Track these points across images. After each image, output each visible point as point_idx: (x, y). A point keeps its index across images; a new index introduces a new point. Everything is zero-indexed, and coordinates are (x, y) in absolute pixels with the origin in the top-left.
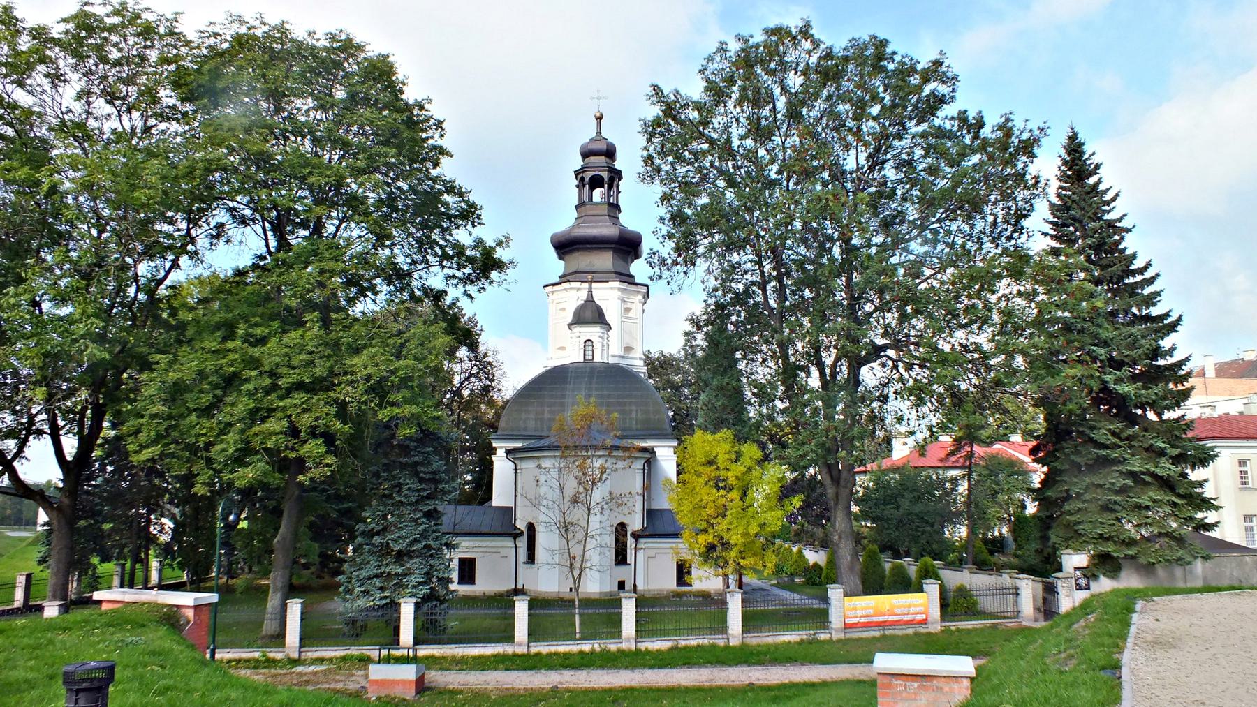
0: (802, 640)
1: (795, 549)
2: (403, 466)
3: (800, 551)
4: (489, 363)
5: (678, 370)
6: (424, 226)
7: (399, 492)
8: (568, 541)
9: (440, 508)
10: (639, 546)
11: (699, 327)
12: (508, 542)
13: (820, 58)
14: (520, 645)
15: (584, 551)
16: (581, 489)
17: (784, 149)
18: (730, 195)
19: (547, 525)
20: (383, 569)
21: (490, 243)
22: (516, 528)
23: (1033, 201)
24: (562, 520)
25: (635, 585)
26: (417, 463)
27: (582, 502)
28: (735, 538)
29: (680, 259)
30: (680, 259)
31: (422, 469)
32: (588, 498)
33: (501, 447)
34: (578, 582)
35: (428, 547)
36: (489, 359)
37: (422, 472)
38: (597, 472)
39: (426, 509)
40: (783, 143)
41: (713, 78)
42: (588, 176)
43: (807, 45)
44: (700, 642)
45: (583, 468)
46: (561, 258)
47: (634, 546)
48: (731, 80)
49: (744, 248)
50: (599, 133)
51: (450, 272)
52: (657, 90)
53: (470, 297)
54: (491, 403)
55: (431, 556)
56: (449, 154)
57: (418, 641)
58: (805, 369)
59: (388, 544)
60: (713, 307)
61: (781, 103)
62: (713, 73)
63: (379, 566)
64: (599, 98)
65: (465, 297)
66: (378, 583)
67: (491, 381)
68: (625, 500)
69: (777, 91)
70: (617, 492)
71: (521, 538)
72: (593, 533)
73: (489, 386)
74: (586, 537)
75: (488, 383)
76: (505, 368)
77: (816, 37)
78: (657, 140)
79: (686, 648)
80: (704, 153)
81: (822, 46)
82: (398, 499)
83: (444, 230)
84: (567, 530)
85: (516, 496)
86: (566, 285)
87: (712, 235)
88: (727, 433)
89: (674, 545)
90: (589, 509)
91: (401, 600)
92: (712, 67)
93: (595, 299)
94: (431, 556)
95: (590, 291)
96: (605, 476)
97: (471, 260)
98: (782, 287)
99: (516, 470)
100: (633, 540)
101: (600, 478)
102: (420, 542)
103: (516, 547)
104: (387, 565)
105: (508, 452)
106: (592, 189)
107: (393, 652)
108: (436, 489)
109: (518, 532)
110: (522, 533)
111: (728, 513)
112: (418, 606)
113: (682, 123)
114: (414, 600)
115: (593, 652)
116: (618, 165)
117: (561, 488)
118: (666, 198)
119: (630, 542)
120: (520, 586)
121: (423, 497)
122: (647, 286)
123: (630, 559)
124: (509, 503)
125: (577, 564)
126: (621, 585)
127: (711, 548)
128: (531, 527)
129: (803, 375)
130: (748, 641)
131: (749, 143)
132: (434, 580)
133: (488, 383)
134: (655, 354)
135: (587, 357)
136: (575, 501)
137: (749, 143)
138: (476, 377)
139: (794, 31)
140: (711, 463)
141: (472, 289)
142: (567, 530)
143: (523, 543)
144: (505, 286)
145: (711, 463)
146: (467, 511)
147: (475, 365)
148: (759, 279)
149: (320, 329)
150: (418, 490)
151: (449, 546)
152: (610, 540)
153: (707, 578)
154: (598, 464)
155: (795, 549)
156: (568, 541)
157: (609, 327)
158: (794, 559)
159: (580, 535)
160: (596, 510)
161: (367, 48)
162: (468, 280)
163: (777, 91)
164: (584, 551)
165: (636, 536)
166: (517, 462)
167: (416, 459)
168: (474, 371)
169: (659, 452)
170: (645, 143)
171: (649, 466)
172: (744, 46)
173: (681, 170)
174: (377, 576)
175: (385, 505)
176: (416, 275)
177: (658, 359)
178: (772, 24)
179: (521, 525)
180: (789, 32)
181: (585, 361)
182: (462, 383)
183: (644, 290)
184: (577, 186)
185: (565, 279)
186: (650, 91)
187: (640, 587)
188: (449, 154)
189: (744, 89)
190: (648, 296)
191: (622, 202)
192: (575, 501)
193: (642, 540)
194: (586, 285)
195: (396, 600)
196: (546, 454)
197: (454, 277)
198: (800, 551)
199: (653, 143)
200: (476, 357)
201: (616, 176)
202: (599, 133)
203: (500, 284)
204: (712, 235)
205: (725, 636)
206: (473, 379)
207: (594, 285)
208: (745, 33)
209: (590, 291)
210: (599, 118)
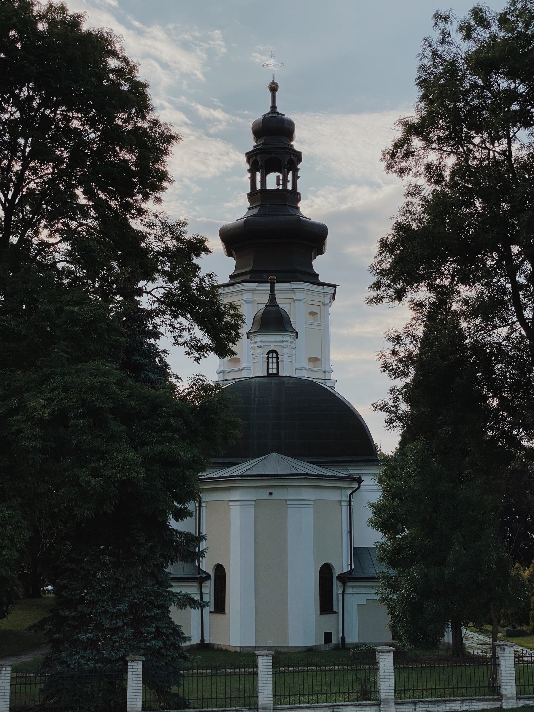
10: (349, 590)
22: (200, 571)
23: (189, 387)
47: (340, 591)
50: (274, 107)
56: (182, 626)
71: (208, 583)
100: (340, 584)
110: (208, 577)
119: (337, 589)
122: (335, 286)
123: (337, 606)
128: (220, 570)
135: (271, 371)
138: (449, 152)
165: (344, 579)
181: (269, 375)
183: (331, 290)
184: (249, 171)
188: (182, 626)
190: (334, 298)
193: (349, 584)
194: (268, 286)
202: (274, 107)
207: (277, 286)
210: (274, 88)
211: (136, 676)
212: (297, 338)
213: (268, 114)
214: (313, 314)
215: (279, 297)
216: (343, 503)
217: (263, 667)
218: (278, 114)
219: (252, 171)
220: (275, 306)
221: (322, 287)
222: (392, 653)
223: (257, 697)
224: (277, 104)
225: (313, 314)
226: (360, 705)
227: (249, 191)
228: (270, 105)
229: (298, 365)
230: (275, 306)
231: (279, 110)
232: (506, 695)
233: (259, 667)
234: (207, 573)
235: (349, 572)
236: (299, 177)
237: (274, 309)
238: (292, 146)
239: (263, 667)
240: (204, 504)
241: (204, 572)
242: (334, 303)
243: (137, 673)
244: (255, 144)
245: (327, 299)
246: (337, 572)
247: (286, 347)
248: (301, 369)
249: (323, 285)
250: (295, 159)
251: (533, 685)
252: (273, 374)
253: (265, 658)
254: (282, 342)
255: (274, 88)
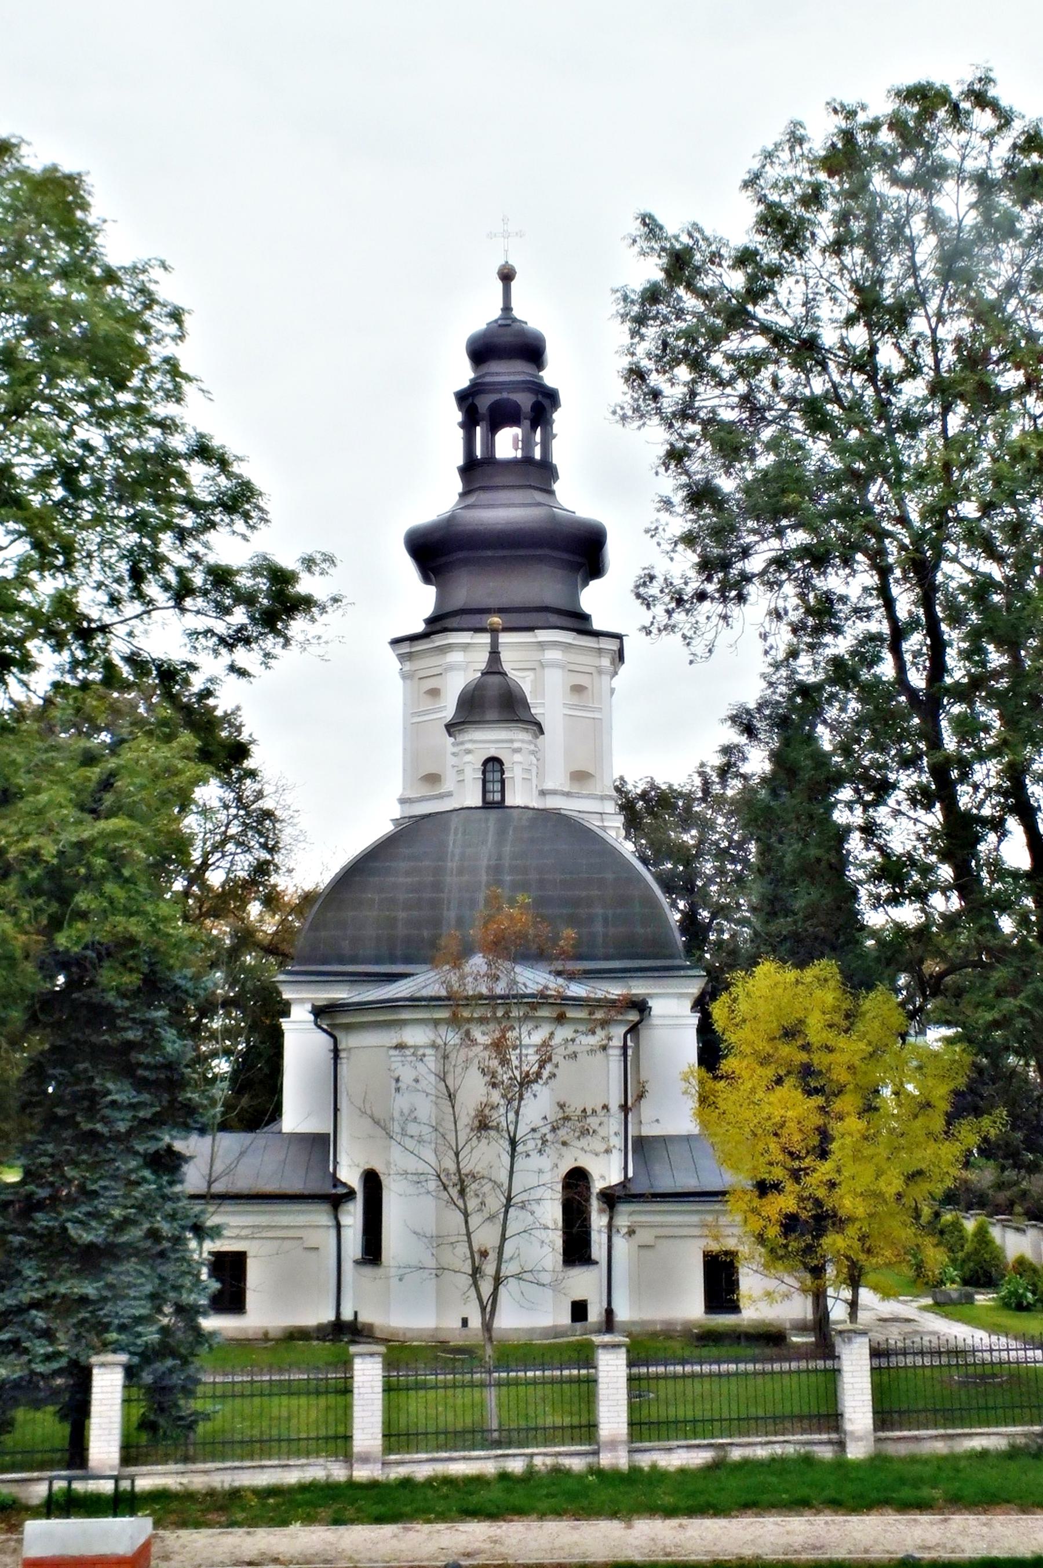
0: (1013, 1446)
1: (970, 1225)
2: (99, 1053)
3: (982, 1233)
4: (268, 814)
5: (688, 820)
6: (139, 523)
7: (91, 1113)
8: (466, 1215)
9: (179, 1146)
11: (749, 730)
12: (321, 1216)
13: (1015, 146)
14: (365, 1459)
15: (503, 1239)
16: (496, 1096)
17: (936, 345)
18: (818, 448)
19: (418, 1179)
20: (52, 1287)
21: (288, 561)
22: (337, 1182)
24: (452, 1167)
25: (609, 1312)
26: (130, 1046)
27: (497, 1128)
28: (848, 1203)
29: (711, 588)
30: (711, 588)
31: (142, 1058)
32: (511, 1116)
33: (302, 1001)
34: (489, 1308)
35: (154, 1235)
36: (267, 804)
37: (140, 1065)
38: (533, 1058)
39: (152, 1147)
40: (934, 331)
41: (774, 197)
42: (484, 402)
43: (984, 120)
44: (778, 1450)
45: (499, 1047)
46: (427, 579)
48: (814, 198)
49: (847, 562)
50: (507, 308)
51: (201, 623)
52: (651, 226)
53: (242, 673)
54: (272, 901)
55: (162, 1254)
57: (131, 1455)
58: (997, 825)
59: (65, 1230)
60: (783, 689)
61: (927, 248)
62: (775, 186)
63: (42, 1281)
64: (506, 235)
65: (234, 676)
66: (40, 1318)
67: (271, 850)
68: (593, 1122)
69: (917, 225)
70: (575, 1107)
72: (524, 1197)
73: (267, 863)
74: (508, 1206)
75: (265, 855)
76: (303, 822)
77: (1004, 103)
78: (651, 331)
79: (746, 1463)
80: (758, 361)
81: (1018, 125)
82: (86, 1126)
83: (182, 535)
84: (462, 1192)
85: (336, 1110)
86: (440, 640)
87: (780, 533)
88: (825, 968)
89: (710, 1218)
90: (513, 1143)
91: (94, 1359)
92: (772, 173)
93: (507, 667)
94: (162, 1254)
95: (495, 654)
96: (549, 1067)
97: (247, 599)
98: (938, 647)
99: (336, 1052)
101: (539, 1075)
102: (134, 1223)
103: (338, 1227)
104: (62, 1279)
105: (319, 1012)
106: (494, 428)
107: (78, 1486)
108: (173, 1101)
109: (341, 1190)
110: (351, 1194)
111: (834, 1146)
112: (131, 1373)
113: (705, 295)
114: (123, 1358)
115: (530, 1474)
116: (549, 377)
117: (451, 1096)
118: (676, 456)
119: (598, 1221)
120: (347, 1315)
121: (143, 1121)
122: (619, 637)
124: (319, 1124)
125: (489, 1268)
126: (579, 1310)
127: (790, 1224)
128: (372, 1181)
129: (992, 837)
130: (893, 1449)
131: (859, 336)
132: (168, 1309)
133: (265, 855)
134: (636, 786)
136: (483, 1125)
137: (859, 336)
138: (239, 844)
139: (955, 93)
140: (790, 1033)
141: (242, 656)
142: (462, 1192)
143: (353, 1216)
144: (313, 649)
145: (790, 1033)
146: (237, 1149)
147: (236, 816)
148: (885, 628)
149: (273, 917)
150: (133, 1106)
151: (200, 1231)
152: (552, 1212)
153: (787, 1296)
154: (538, 1037)
155: (970, 1225)
156: (466, 1215)
157: (538, 728)
158: (968, 1247)
159: (495, 1203)
160: (531, 1145)
161: (24, 150)
162: (239, 638)
163: (917, 225)
164: (503, 1239)
165: (611, 1199)
166: (340, 1035)
167: (130, 1035)
168: (233, 830)
169: (657, 1007)
170: (627, 340)
171: (637, 1040)
172: (843, 124)
173: (708, 397)
174: (36, 1305)
175: (59, 1141)
176: (121, 630)
177: (644, 796)
178: (910, 79)
179: (350, 1175)
180: (942, 96)
182: (206, 856)
183: (612, 645)
185: (438, 626)
186: (636, 228)
187: (623, 1314)
189: (843, 218)
191: (559, 457)
192: (483, 1125)
193: (623, 1208)
194: (485, 638)
195: (82, 1359)
196: (405, 1015)
197: (209, 632)
198: (982, 1233)
199: (642, 338)
200: (239, 799)
201: (546, 402)
202: (507, 308)
203: (304, 645)
204: (780, 533)
205: (834, 1436)
206: (230, 847)
207: (504, 638)
208: (850, 101)
209: (495, 654)
210: (507, 276)
211: (109, 1396)
212: (542, 732)
213: (496, 321)
214: (578, 689)
215: (509, 660)
216: (611, 1052)
217: (365, 1378)
218: (515, 320)
219: (469, 424)
220: (500, 673)
221: (594, 639)
222: (624, 1350)
223: (384, 1436)
224: (514, 304)
225: (578, 689)
226: (698, 1446)
227: (460, 461)
228: (501, 305)
229: (549, 785)
230: (500, 673)
231: (517, 313)
232: (852, 1433)
233: (600, 1368)
234: (350, 1187)
235: (623, 1185)
236: (554, 436)
237: (495, 679)
238: (541, 378)
239: (365, 1378)
240: (343, 1055)
241: (344, 1185)
242: (623, 670)
243: (110, 1389)
244: (472, 375)
245: (606, 662)
246: (598, 1185)
247: (518, 751)
248: (554, 792)
249: (597, 634)
250: (546, 402)
251: (1039, 1407)
252: (494, 803)
253: (369, 1359)
254: (512, 741)
255: (507, 276)
